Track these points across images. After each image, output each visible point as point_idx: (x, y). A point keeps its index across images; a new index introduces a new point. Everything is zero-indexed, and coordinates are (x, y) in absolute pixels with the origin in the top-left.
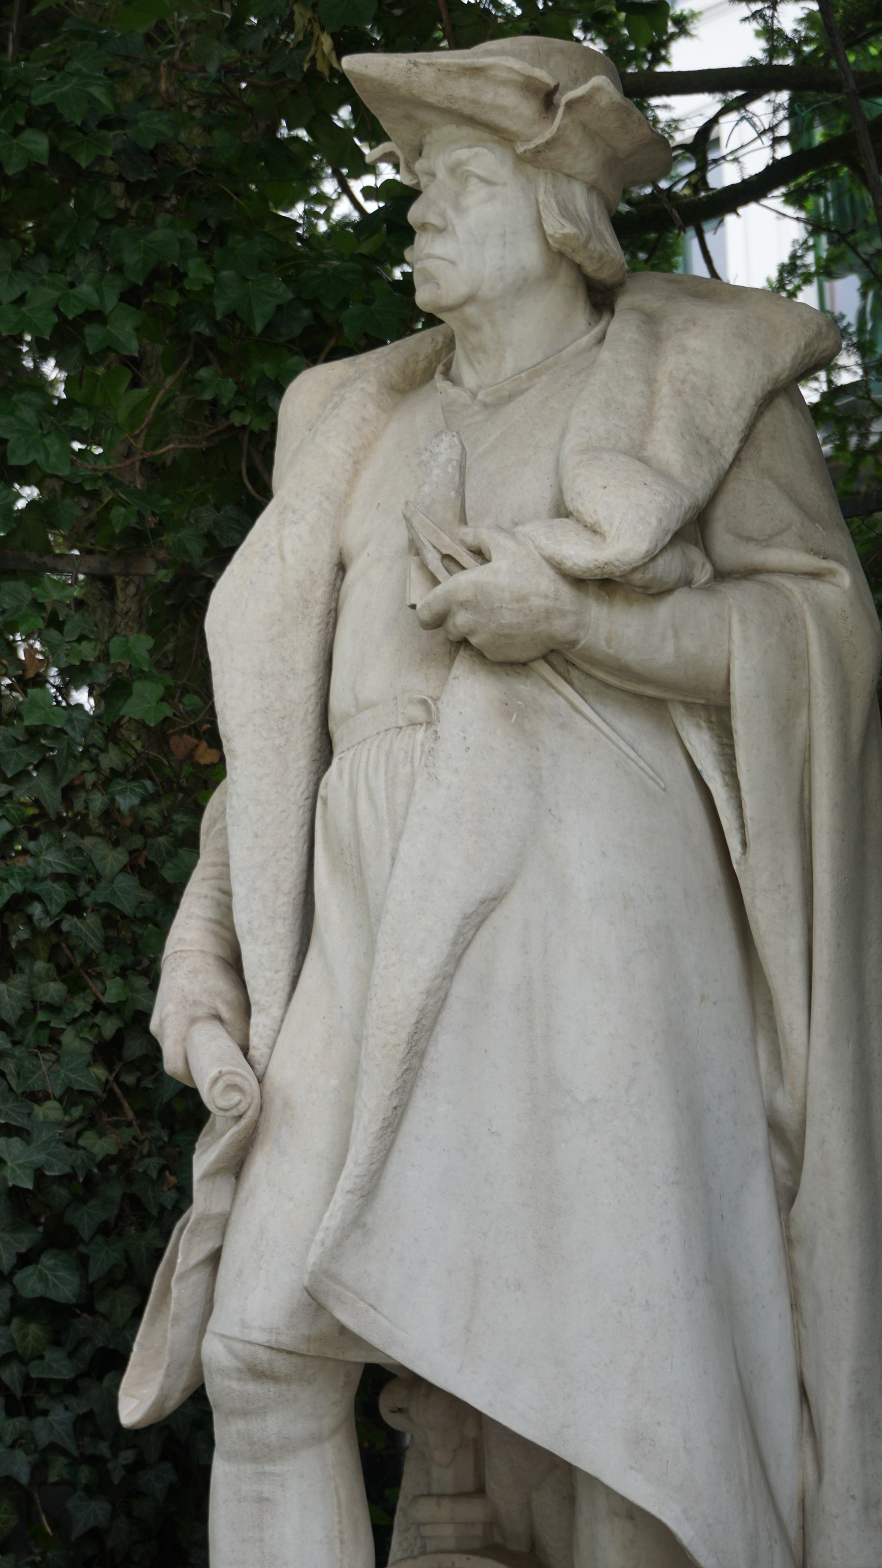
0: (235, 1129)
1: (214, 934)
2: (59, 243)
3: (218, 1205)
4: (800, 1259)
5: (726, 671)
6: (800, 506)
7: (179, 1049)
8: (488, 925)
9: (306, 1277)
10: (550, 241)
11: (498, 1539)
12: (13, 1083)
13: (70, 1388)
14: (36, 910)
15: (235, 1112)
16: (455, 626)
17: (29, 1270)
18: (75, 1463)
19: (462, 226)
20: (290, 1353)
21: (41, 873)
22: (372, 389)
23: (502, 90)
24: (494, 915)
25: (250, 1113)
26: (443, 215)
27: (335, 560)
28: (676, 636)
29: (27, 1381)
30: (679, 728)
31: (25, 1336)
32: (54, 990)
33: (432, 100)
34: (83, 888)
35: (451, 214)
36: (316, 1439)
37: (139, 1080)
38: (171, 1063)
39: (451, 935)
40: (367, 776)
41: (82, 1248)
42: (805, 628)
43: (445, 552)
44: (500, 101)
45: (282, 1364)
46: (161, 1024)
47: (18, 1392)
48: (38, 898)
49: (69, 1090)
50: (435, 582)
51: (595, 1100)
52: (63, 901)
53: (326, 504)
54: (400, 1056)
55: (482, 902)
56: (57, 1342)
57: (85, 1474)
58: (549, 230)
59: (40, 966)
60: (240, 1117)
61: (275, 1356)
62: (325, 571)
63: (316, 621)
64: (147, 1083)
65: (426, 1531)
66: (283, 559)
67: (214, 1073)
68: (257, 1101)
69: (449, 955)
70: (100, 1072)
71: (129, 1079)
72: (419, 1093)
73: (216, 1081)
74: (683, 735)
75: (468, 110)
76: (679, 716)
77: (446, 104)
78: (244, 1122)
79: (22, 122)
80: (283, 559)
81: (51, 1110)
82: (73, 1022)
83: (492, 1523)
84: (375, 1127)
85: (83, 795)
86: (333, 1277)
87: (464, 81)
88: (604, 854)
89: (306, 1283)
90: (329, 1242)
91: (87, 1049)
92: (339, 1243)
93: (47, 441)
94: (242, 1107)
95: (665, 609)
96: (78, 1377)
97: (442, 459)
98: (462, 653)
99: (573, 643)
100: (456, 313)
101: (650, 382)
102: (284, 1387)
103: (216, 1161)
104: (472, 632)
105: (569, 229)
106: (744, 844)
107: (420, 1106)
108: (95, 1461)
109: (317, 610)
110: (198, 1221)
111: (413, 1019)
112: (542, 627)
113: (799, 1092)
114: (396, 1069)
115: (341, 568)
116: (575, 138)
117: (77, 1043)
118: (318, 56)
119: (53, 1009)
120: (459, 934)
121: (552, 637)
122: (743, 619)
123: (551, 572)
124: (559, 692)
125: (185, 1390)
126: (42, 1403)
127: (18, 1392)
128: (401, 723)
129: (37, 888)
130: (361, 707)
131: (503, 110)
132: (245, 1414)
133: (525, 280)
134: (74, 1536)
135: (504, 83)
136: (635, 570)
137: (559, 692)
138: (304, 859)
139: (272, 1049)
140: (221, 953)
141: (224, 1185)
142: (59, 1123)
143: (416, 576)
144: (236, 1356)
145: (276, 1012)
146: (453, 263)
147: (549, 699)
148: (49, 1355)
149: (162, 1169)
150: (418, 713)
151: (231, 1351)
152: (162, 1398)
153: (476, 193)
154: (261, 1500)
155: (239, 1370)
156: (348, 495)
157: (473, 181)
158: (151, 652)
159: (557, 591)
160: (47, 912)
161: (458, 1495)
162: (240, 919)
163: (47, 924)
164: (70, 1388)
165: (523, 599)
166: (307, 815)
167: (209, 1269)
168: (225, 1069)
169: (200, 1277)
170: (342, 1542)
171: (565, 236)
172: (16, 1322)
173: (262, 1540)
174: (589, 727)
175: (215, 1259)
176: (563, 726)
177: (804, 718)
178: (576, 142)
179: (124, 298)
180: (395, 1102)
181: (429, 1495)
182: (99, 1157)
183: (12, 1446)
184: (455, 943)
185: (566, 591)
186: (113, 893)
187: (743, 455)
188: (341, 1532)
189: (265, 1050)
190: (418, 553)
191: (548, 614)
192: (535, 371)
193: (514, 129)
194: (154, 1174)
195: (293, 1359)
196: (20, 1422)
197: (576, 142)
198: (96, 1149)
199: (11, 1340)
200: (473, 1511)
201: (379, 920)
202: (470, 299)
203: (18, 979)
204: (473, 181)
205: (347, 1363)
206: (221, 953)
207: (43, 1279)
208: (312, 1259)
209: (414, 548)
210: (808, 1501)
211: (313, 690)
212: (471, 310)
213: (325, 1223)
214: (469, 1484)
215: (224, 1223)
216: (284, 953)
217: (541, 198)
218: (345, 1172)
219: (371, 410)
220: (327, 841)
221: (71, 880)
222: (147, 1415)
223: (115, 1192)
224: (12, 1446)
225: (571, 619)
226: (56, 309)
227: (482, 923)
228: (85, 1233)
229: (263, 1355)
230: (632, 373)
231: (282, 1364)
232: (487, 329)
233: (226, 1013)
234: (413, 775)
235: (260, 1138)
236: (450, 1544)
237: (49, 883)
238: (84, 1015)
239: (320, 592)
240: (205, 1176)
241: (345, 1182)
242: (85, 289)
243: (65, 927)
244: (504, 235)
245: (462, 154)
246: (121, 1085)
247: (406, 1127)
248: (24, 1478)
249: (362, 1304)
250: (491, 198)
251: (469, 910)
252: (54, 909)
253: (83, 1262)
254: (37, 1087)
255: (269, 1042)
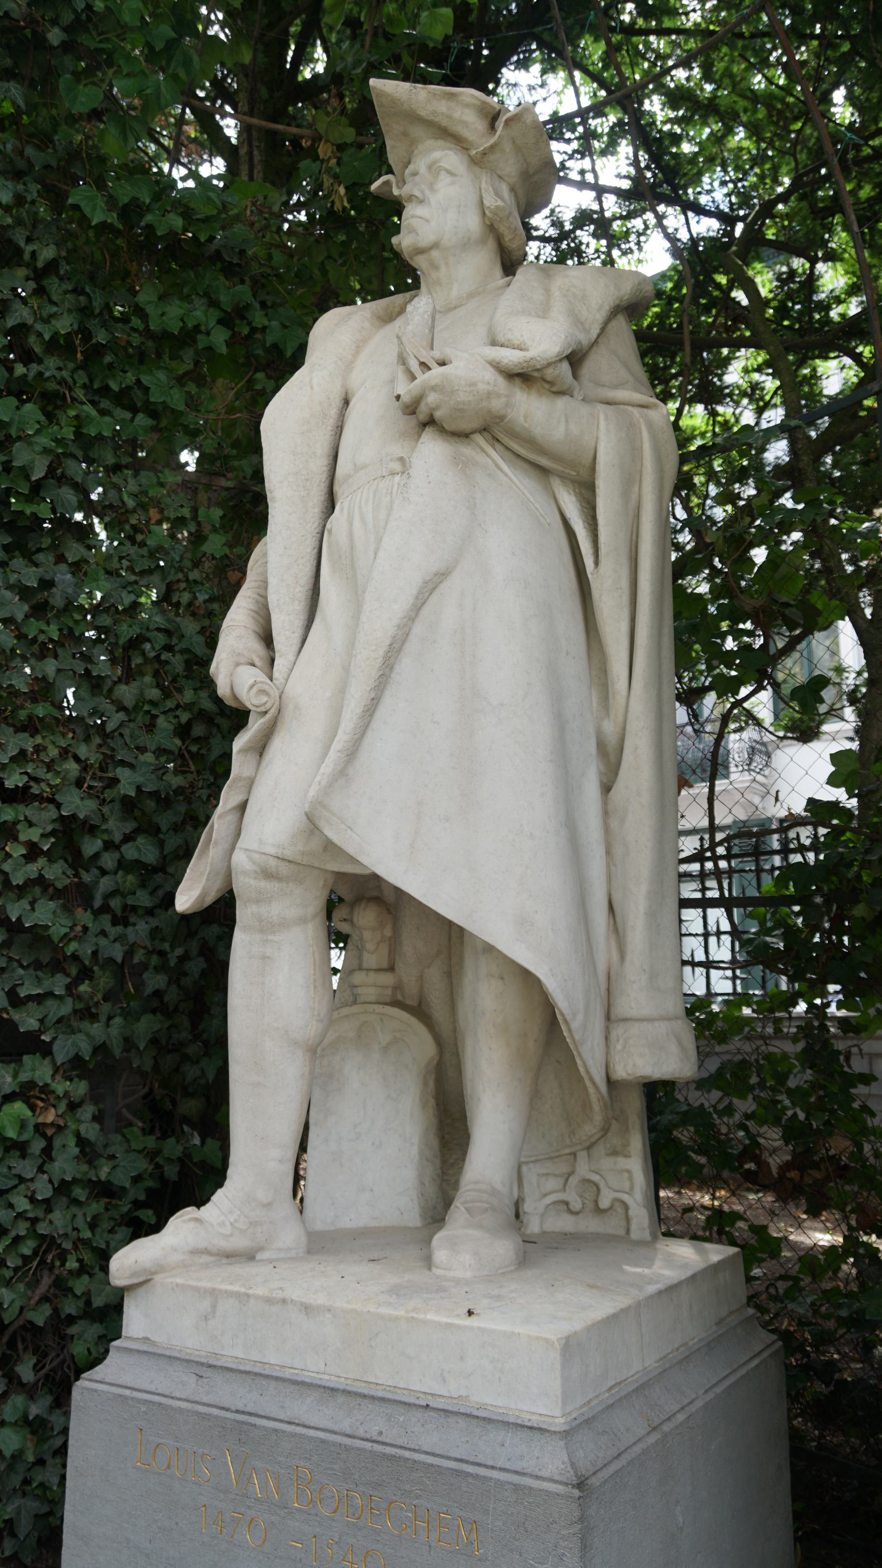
0: (262, 720)
1: (253, 617)
2: (185, 291)
3: (248, 772)
4: (614, 824)
5: (592, 452)
6: (633, 375)
7: (228, 681)
8: (438, 591)
9: (307, 805)
10: (487, 212)
11: (400, 997)
12: (128, 741)
13: (150, 912)
14: (147, 646)
15: (263, 709)
16: (427, 404)
17: (130, 844)
18: (150, 953)
19: (433, 199)
20: (290, 862)
21: (151, 627)
22: (368, 315)
23: (467, 111)
24: (442, 586)
25: (272, 711)
26: (423, 192)
27: (343, 395)
28: (567, 421)
29: (125, 907)
30: (557, 492)
31: (125, 882)
32: (154, 693)
33: (423, 113)
34: (175, 641)
35: (427, 192)
36: (303, 921)
37: (199, 749)
38: (223, 690)
39: (415, 592)
40: (360, 507)
41: (161, 836)
42: (641, 433)
43: (422, 360)
44: (464, 118)
45: (284, 869)
46: (217, 667)
47: (119, 913)
48: (149, 640)
49: (159, 749)
50: (413, 378)
51: (502, 705)
52: (163, 643)
53: (339, 363)
54: (378, 665)
55: (436, 575)
56: (143, 885)
57: (155, 960)
58: (487, 203)
59: (148, 679)
60: (266, 712)
61: (280, 863)
62: (337, 402)
63: (329, 428)
64: (203, 751)
65: (356, 991)
66: (312, 388)
67: (251, 681)
68: (277, 703)
69: (413, 605)
70: (178, 742)
71: (194, 749)
72: (387, 694)
73: (252, 686)
74: (559, 497)
75: (444, 123)
76: (558, 487)
77: (431, 118)
78: (268, 716)
79: (169, 209)
80: (312, 388)
81: (149, 757)
82: (165, 713)
83: (398, 987)
84: (359, 711)
85: (178, 594)
86: (324, 807)
87: (443, 102)
88: (513, 554)
89: (307, 809)
90: (324, 783)
91: (171, 727)
92: (330, 785)
93: (172, 392)
94: (268, 706)
95: (561, 403)
96: (155, 907)
97: (421, 310)
98: (427, 429)
99: (502, 418)
100: (425, 256)
101: (547, 291)
102: (284, 885)
103: (249, 741)
104: (437, 408)
105: (500, 203)
106: (597, 563)
107: (388, 700)
108: (162, 954)
109: (331, 422)
110: (234, 781)
111: (388, 643)
112: (484, 404)
113: (620, 719)
114: (375, 674)
115: (346, 402)
116: (507, 147)
117: (165, 724)
118: (337, 200)
119: (152, 703)
120: (420, 592)
121: (489, 412)
122: (606, 419)
123: (492, 370)
124: (488, 455)
125: (218, 891)
126: (132, 919)
127: (119, 913)
128: (384, 474)
129: (148, 635)
130: (357, 469)
131: (465, 124)
132: (257, 901)
133: (469, 239)
134: (146, 994)
135: (467, 106)
136: (549, 365)
137: (488, 455)
138: (314, 569)
139: (287, 680)
140: (257, 630)
141: (252, 758)
142: (151, 764)
143: (401, 377)
144: (254, 863)
145: (291, 658)
146: (427, 221)
147: (481, 458)
148: (138, 893)
149: (209, 796)
150: (397, 466)
151: (251, 859)
152: (203, 896)
153: (444, 180)
154: (265, 958)
155: (255, 872)
156: (352, 362)
157: (443, 173)
158: (222, 518)
159: (496, 380)
160: (153, 648)
161: (379, 970)
162: (272, 599)
163: (153, 654)
164: (150, 912)
165: (473, 384)
166: (317, 543)
167: (239, 814)
168: (258, 680)
169: (232, 818)
170: (315, 987)
171: (497, 207)
172: (120, 873)
173: (263, 983)
174: (506, 479)
175: (243, 807)
176: (489, 475)
177: (637, 489)
178: (508, 150)
179: (220, 322)
180: (373, 695)
181: (360, 969)
182: (174, 787)
183: (115, 941)
184: (417, 598)
185: (501, 381)
186: (191, 644)
187: (600, 340)
188: (315, 981)
189: (283, 681)
190: (404, 364)
191: (489, 395)
192: (471, 296)
193: (471, 139)
194: (205, 798)
195: (292, 866)
196: (119, 929)
197: (508, 150)
198: (173, 782)
199: (117, 883)
200: (387, 979)
201: (364, 592)
202: (435, 246)
203: (135, 684)
204: (443, 173)
205: (327, 871)
206: (257, 630)
207: (138, 849)
208: (312, 793)
209: (402, 360)
210: (612, 973)
211: (325, 469)
212: (435, 254)
213: (322, 770)
214: (385, 965)
215: (251, 783)
216: (299, 622)
217: (483, 186)
218: (337, 738)
219: (367, 325)
220: (329, 547)
221: (168, 632)
222: (193, 905)
223: (182, 808)
224: (115, 941)
225: (503, 400)
226: (182, 320)
227: (434, 589)
228: (164, 828)
229: (273, 862)
230: (536, 285)
231: (284, 869)
232: (443, 268)
233: (258, 662)
234: (392, 502)
235: (278, 729)
236: (372, 998)
237: (156, 633)
238: (170, 710)
239: (334, 412)
240: (239, 751)
241: (337, 745)
242: (198, 313)
243: (163, 657)
244: (459, 206)
245: (437, 154)
246: (189, 752)
247: (378, 714)
248: (119, 960)
249: (343, 826)
250: (453, 183)
251: (428, 578)
252: (157, 647)
253: (161, 844)
254: (141, 745)
255: (286, 676)
